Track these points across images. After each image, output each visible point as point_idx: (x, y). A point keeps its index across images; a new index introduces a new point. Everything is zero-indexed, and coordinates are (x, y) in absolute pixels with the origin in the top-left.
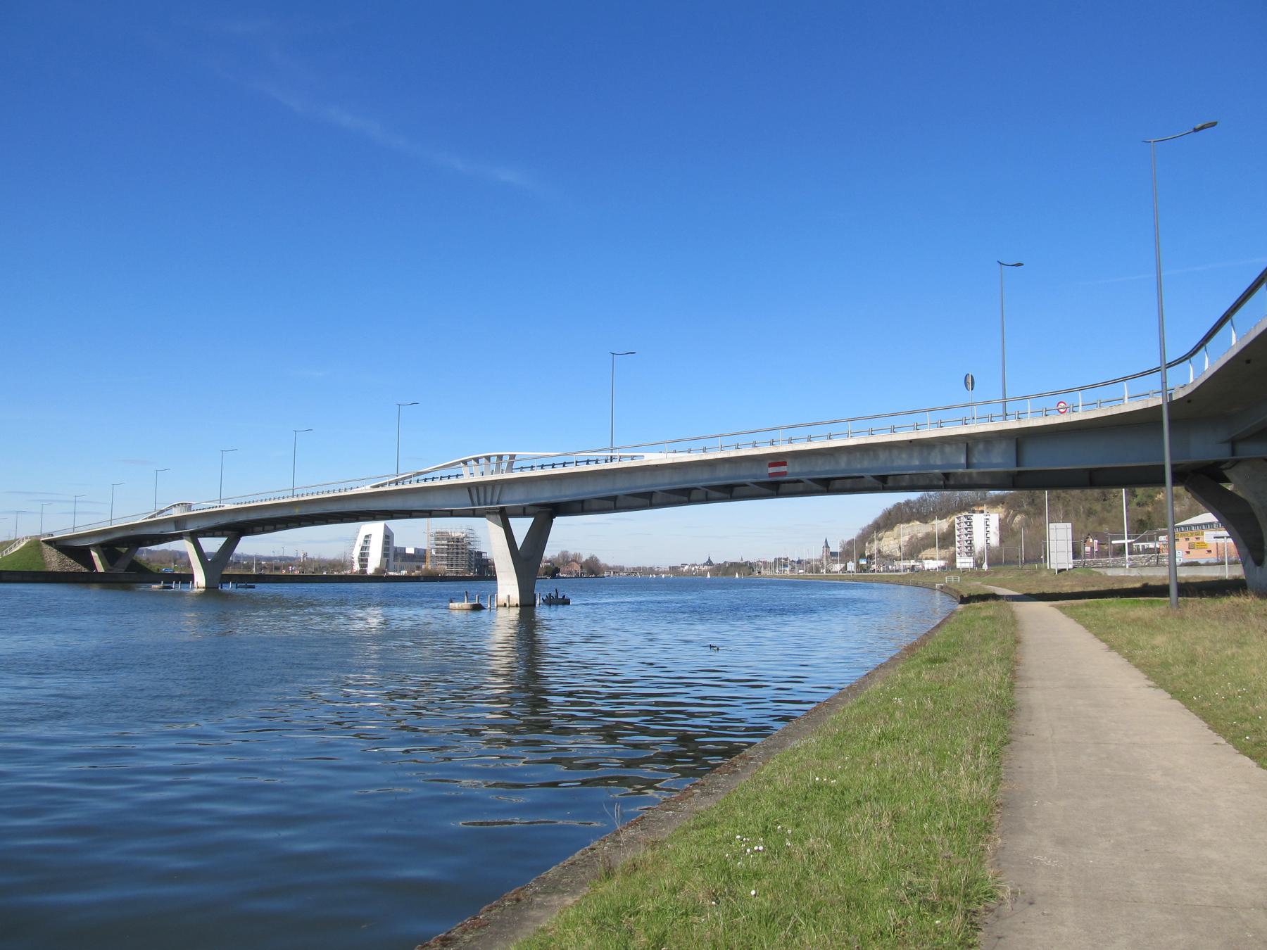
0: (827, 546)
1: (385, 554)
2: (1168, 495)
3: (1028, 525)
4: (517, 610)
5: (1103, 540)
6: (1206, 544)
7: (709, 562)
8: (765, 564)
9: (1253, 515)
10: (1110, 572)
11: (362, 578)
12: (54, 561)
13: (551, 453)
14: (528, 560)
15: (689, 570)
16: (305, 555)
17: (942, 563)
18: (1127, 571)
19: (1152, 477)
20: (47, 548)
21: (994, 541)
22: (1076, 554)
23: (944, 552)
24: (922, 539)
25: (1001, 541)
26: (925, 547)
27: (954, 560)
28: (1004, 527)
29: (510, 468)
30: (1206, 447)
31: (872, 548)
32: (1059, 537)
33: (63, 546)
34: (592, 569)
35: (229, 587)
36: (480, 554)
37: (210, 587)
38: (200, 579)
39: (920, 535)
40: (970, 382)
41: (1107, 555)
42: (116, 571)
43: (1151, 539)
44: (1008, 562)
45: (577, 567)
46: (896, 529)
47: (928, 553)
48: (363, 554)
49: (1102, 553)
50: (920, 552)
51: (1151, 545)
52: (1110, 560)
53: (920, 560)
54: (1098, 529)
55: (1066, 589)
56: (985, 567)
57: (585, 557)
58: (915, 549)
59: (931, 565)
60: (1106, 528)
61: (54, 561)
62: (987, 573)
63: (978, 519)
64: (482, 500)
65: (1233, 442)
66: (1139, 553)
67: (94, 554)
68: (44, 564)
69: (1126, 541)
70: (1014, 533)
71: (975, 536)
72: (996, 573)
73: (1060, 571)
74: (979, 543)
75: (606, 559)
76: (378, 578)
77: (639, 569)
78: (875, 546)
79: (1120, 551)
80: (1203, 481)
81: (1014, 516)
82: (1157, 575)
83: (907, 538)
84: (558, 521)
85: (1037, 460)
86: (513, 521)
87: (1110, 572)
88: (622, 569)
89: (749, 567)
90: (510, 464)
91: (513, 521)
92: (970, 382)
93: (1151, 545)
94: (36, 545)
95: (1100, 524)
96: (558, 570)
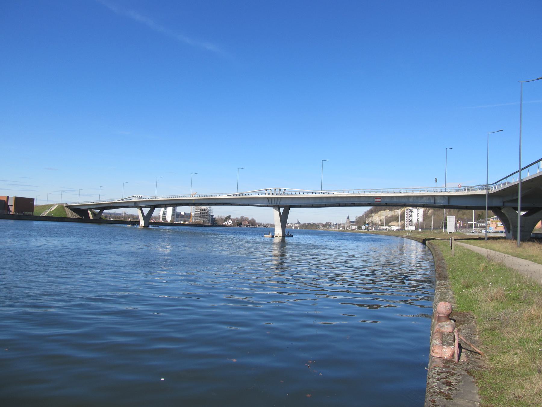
0: (348, 218)
1: (173, 215)
2: (486, 212)
3: (434, 214)
4: (281, 238)
5: (464, 221)
6: (496, 226)
7: (299, 223)
8: (323, 225)
9: (507, 220)
10: (468, 234)
11: (166, 224)
12: (70, 214)
13: (298, 190)
14: (147, 218)
15: (290, 226)
16: (125, 213)
17: (398, 228)
18: (473, 233)
19: (483, 208)
20: (66, 209)
21: (421, 220)
22: (456, 227)
23: (399, 223)
24: (390, 217)
25: (423, 220)
26: (392, 221)
27: (404, 227)
28: (425, 214)
29: (284, 193)
30: (497, 203)
31: (369, 220)
32: (451, 220)
33: (73, 209)
34: (253, 223)
35: (151, 226)
36: (212, 216)
37: (146, 226)
38: (142, 223)
39: (389, 216)
40: (436, 180)
41: (466, 227)
42: (96, 218)
43: (483, 222)
44: (427, 229)
45: (247, 223)
46: (379, 213)
47: (393, 223)
48: (164, 214)
49: (464, 227)
50: (390, 222)
51: (483, 225)
52: (466, 229)
53: (390, 226)
54: (462, 217)
55: (459, 238)
56: (420, 230)
57: (250, 218)
58: (388, 221)
59: (394, 228)
60: (465, 217)
61: (70, 214)
62: (421, 232)
63: (415, 210)
64: (270, 202)
65: (504, 202)
66: (478, 227)
67: (89, 212)
68: (66, 215)
69: (473, 223)
70: (429, 217)
71: (413, 217)
72: (425, 232)
73: (450, 233)
74: (414, 221)
75: (257, 221)
76: (172, 224)
77: (268, 224)
78: (370, 219)
79: (471, 226)
80: (497, 210)
81: (429, 210)
82: (483, 233)
83: (384, 217)
84: (291, 209)
85: (453, 203)
86: (280, 208)
87: (468, 234)
88: (261, 224)
89: (316, 226)
90: (284, 193)
91: (280, 208)
92: (436, 180)
93: (483, 225)
94: (62, 207)
95: (463, 215)
96: (241, 224)
